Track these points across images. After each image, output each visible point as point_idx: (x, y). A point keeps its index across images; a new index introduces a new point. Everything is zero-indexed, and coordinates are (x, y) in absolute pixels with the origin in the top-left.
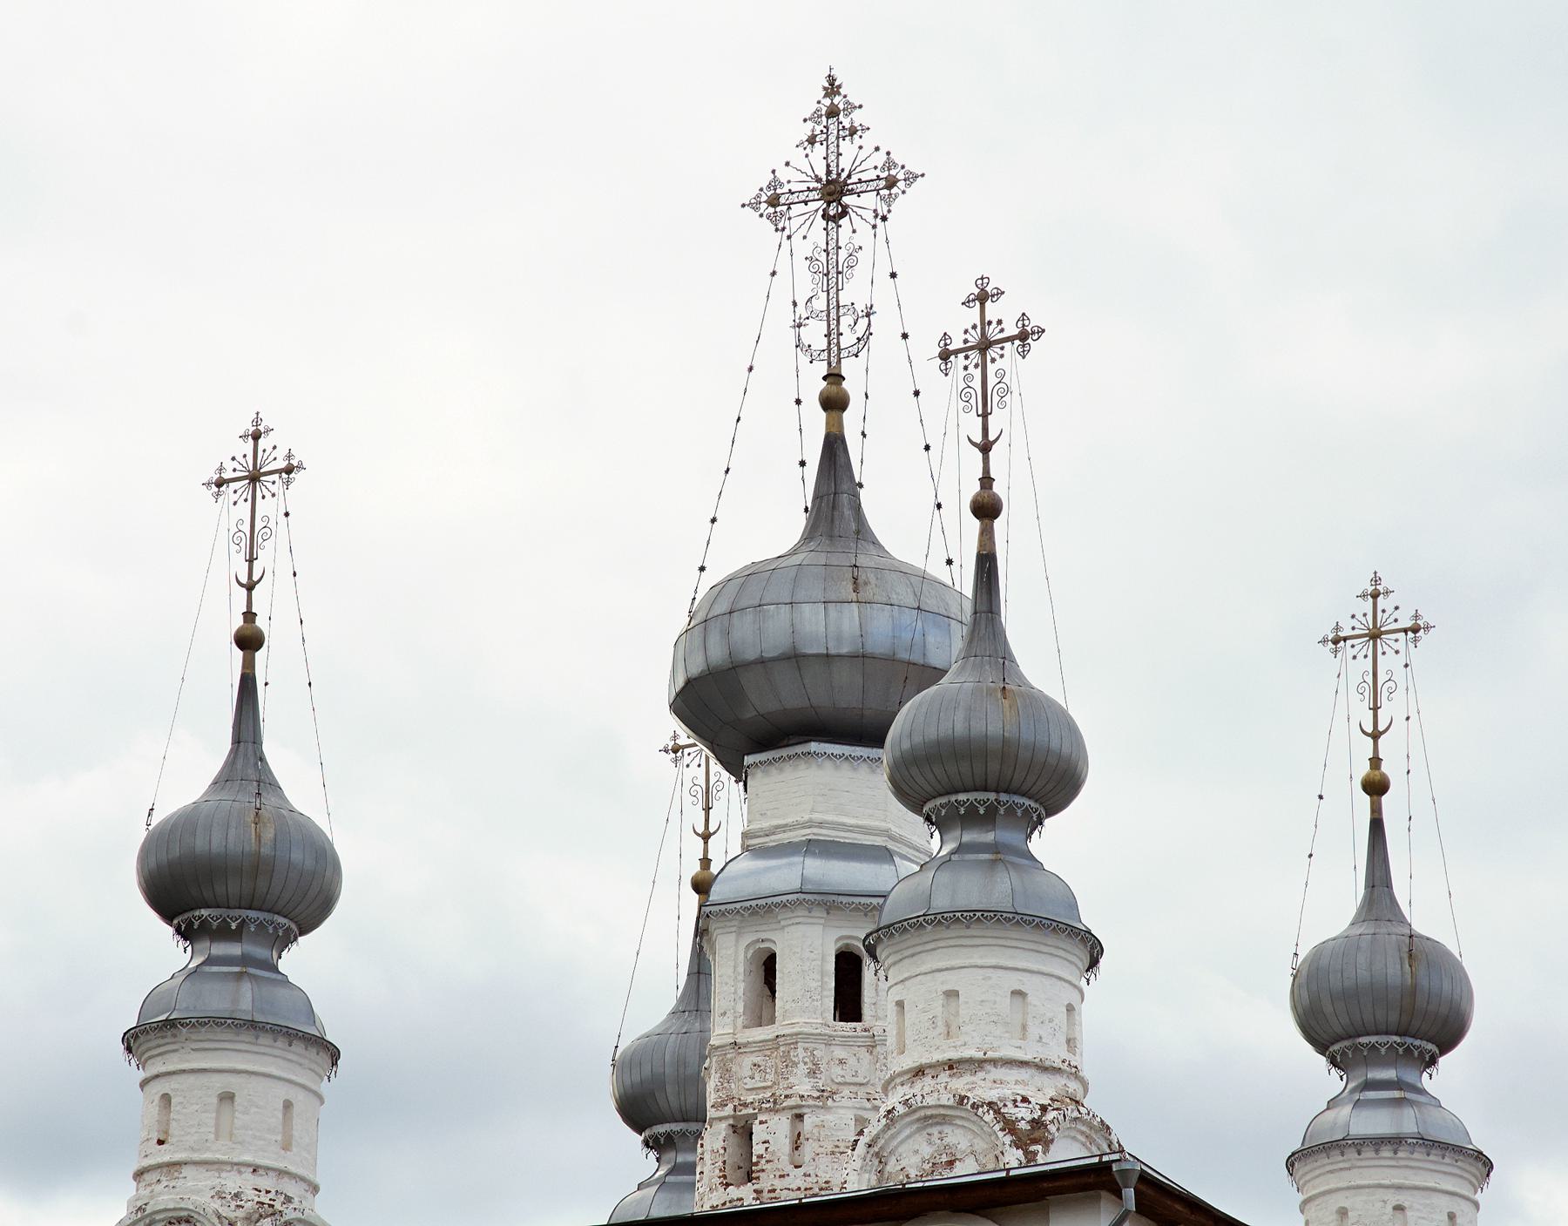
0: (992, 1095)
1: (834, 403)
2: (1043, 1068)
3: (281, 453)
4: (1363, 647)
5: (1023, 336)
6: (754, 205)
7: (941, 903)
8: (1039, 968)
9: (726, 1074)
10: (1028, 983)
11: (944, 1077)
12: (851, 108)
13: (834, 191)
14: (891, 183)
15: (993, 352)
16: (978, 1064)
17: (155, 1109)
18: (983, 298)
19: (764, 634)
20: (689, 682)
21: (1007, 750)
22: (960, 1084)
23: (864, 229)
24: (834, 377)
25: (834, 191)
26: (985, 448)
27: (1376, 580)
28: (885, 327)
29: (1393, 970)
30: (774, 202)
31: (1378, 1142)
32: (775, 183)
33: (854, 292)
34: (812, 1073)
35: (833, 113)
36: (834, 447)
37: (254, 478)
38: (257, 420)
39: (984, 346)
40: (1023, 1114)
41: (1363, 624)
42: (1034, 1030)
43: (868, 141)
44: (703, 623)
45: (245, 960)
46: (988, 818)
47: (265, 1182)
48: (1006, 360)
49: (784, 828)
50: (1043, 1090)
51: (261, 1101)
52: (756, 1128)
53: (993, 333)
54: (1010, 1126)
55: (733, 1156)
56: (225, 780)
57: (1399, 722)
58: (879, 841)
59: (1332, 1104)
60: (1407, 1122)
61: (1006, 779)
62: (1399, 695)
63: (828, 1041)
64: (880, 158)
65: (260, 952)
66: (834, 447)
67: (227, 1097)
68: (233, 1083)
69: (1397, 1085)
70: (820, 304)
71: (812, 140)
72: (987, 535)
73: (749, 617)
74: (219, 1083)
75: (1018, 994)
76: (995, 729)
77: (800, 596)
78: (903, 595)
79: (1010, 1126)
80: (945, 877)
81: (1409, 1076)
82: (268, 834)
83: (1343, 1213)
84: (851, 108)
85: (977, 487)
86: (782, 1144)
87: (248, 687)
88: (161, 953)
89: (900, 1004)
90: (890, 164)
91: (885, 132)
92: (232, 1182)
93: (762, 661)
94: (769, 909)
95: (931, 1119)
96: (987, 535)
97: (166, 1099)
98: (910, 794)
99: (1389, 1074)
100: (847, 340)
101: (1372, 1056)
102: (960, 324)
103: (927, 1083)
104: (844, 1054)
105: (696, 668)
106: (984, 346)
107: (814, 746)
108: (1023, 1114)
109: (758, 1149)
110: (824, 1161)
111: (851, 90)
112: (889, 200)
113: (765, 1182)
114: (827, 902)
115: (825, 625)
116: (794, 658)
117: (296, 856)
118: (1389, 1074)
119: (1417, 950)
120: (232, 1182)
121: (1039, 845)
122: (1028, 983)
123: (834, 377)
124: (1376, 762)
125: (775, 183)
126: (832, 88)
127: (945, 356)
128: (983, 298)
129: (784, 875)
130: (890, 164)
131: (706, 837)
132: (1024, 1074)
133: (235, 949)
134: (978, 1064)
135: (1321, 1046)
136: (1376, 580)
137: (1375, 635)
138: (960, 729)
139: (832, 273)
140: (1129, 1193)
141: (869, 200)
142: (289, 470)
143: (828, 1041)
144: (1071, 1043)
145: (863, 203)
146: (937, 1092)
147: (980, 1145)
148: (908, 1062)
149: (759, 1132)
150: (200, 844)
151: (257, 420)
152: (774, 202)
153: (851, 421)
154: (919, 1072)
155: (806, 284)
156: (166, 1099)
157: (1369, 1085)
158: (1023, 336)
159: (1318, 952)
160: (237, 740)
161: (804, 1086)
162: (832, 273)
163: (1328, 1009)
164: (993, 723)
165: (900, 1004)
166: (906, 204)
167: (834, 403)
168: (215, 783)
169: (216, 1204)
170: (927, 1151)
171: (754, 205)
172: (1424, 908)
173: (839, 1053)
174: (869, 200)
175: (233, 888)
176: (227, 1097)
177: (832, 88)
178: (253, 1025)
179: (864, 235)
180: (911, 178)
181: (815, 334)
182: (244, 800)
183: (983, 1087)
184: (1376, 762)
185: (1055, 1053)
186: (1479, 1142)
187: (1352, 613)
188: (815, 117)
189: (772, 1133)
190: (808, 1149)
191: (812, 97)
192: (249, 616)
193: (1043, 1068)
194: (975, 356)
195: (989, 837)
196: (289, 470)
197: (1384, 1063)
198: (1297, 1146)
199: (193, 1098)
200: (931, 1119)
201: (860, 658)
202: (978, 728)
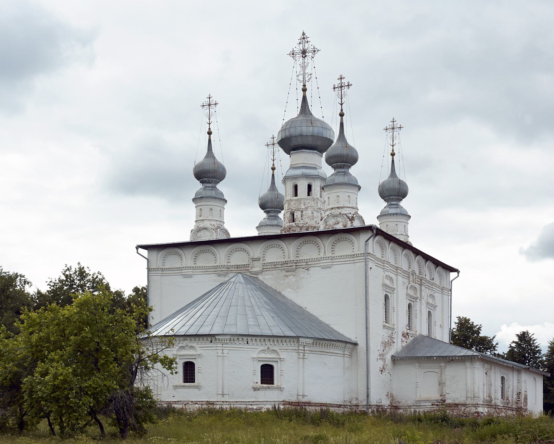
0: (345, 213)
1: (304, 90)
2: (353, 208)
3: (214, 101)
4: (391, 131)
5: (348, 85)
6: (290, 55)
7: (336, 181)
8: (351, 191)
9: (289, 204)
10: (350, 194)
11: (337, 209)
12: (307, 38)
13: (304, 52)
14: (315, 51)
15: (343, 88)
16: (342, 208)
17: (199, 211)
18: (341, 78)
19: (294, 132)
20: (282, 139)
21: (347, 156)
22: (340, 211)
23: (310, 60)
24: (304, 86)
25: (304, 52)
26: (342, 104)
27: (394, 119)
28: (314, 76)
29: (397, 186)
30: (293, 54)
31: (394, 214)
32: (293, 51)
33: (308, 71)
34: (304, 205)
35: (304, 38)
36: (304, 98)
37: (209, 105)
38: (210, 95)
39: (341, 87)
40: (350, 216)
41: (391, 127)
42: (351, 202)
43: (310, 44)
44: (283, 129)
45: (212, 187)
46: (343, 167)
47: (218, 223)
48: (345, 89)
49: (298, 164)
50: (353, 211)
51: (216, 209)
52: (295, 214)
53: (343, 85)
54: (348, 218)
55: (291, 218)
56: (207, 157)
57: (397, 143)
58: (314, 166)
59: (385, 207)
60: (398, 211)
61: (344, 160)
62: (398, 139)
63: (307, 199)
64: (312, 47)
65: (214, 185)
66: (304, 98)
67: (211, 209)
68: (212, 207)
69: (396, 205)
70: (302, 72)
71: (300, 43)
72: (342, 119)
73: (293, 129)
74: (210, 207)
75: (349, 196)
76: (345, 153)
77: (302, 125)
78: (319, 125)
79: (348, 218)
80: (337, 177)
81: (398, 203)
82: (216, 166)
83: (387, 225)
84: (307, 38)
85: (340, 111)
86: (299, 216)
87: (210, 141)
88: (198, 186)
89: (329, 198)
90: (314, 48)
91: (313, 42)
92: (213, 223)
93: (296, 136)
94: (294, 178)
95: (335, 216)
96: (342, 119)
97: (201, 209)
98: (329, 161)
99: (395, 203)
100: (307, 79)
101: (392, 200)
102: (337, 83)
103: (334, 210)
104: (310, 202)
105: (283, 137)
106: (341, 87)
107: (304, 150)
108: (350, 216)
109: (295, 217)
110: (307, 219)
111: (307, 34)
112: (314, 54)
113: (297, 222)
114: (306, 176)
115: (306, 130)
116: (301, 135)
117: (221, 170)
118: (395, 203)
119: (401, 183)
120: (213, 223)
121: (218, 186)
122: (350, 194)
123: (304, 86)
124: (393, 150)
125: (293, 51)
126: (304, 34)
127: (334, 88)
128: (341, 78)
129: (299, 172)
130: (314, 48)
131: (273, 160)
132: (350, 209)
133: (210, 185)
134: (342, 208)
135: (383, 198)
136: (394, 119)
137: (393, 129)
138: (339, 152)
139: (304, 67)
140: (375, 231)
141: (311, 54)
142: (216, 104)
143: (307, 199)
144: (357, 204)
145: (309, 55)
146: (336, 212)
147: (343, 220)
148: (330, 207)
149: (295, 214)
150: (205, 168)
151: (210, 95)
152: (293, 54)
153: (307, 93)
154: (332, 208)
155: (299, 69)
156: (201, 209)
157: (391, 205)
158: (348, 85)
159: (383, 183)
160: (208, 150)
161: (303, 207)
162: (304, 67)
163: (385, 192)
164: (345, 152)
165: (329, 198)
166: (317, 55)
167: (304, 90)
168: (205, 157)
169: (210, 226)
170: (334, 221)
171: (290, 55)
172: (401, 175)
173: (309, 201)
174: (311, 54)
175: (211, 175)
176: (211, 209)
177: (304, 34)
178: (215, 198)
179: (310, 60)
180: (318, 51)
181: (301, 78)
182: (211, 161)
183: (344, 211)
184: (393, 150)
185: (354, 206)
186: (409, 214)
187: (389, 125)
188: (300, 39)
189: (297, 215)
190: (304, 217)
191: (300, 35)
192: (210, 129)
193: (353, 208)
194: (340, 88)
195: (343, 170)
196: (216, 104)
197: (394, 201)
198: (379, 214)
199: (206, 210)
200: (335, 216)
201: (312, 136)
202: (342, 153)
